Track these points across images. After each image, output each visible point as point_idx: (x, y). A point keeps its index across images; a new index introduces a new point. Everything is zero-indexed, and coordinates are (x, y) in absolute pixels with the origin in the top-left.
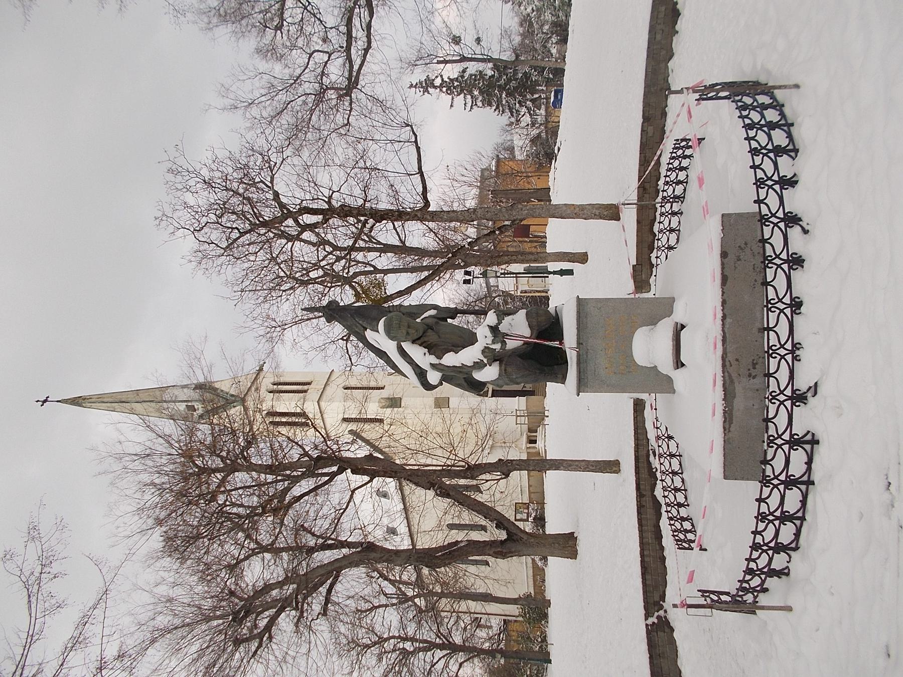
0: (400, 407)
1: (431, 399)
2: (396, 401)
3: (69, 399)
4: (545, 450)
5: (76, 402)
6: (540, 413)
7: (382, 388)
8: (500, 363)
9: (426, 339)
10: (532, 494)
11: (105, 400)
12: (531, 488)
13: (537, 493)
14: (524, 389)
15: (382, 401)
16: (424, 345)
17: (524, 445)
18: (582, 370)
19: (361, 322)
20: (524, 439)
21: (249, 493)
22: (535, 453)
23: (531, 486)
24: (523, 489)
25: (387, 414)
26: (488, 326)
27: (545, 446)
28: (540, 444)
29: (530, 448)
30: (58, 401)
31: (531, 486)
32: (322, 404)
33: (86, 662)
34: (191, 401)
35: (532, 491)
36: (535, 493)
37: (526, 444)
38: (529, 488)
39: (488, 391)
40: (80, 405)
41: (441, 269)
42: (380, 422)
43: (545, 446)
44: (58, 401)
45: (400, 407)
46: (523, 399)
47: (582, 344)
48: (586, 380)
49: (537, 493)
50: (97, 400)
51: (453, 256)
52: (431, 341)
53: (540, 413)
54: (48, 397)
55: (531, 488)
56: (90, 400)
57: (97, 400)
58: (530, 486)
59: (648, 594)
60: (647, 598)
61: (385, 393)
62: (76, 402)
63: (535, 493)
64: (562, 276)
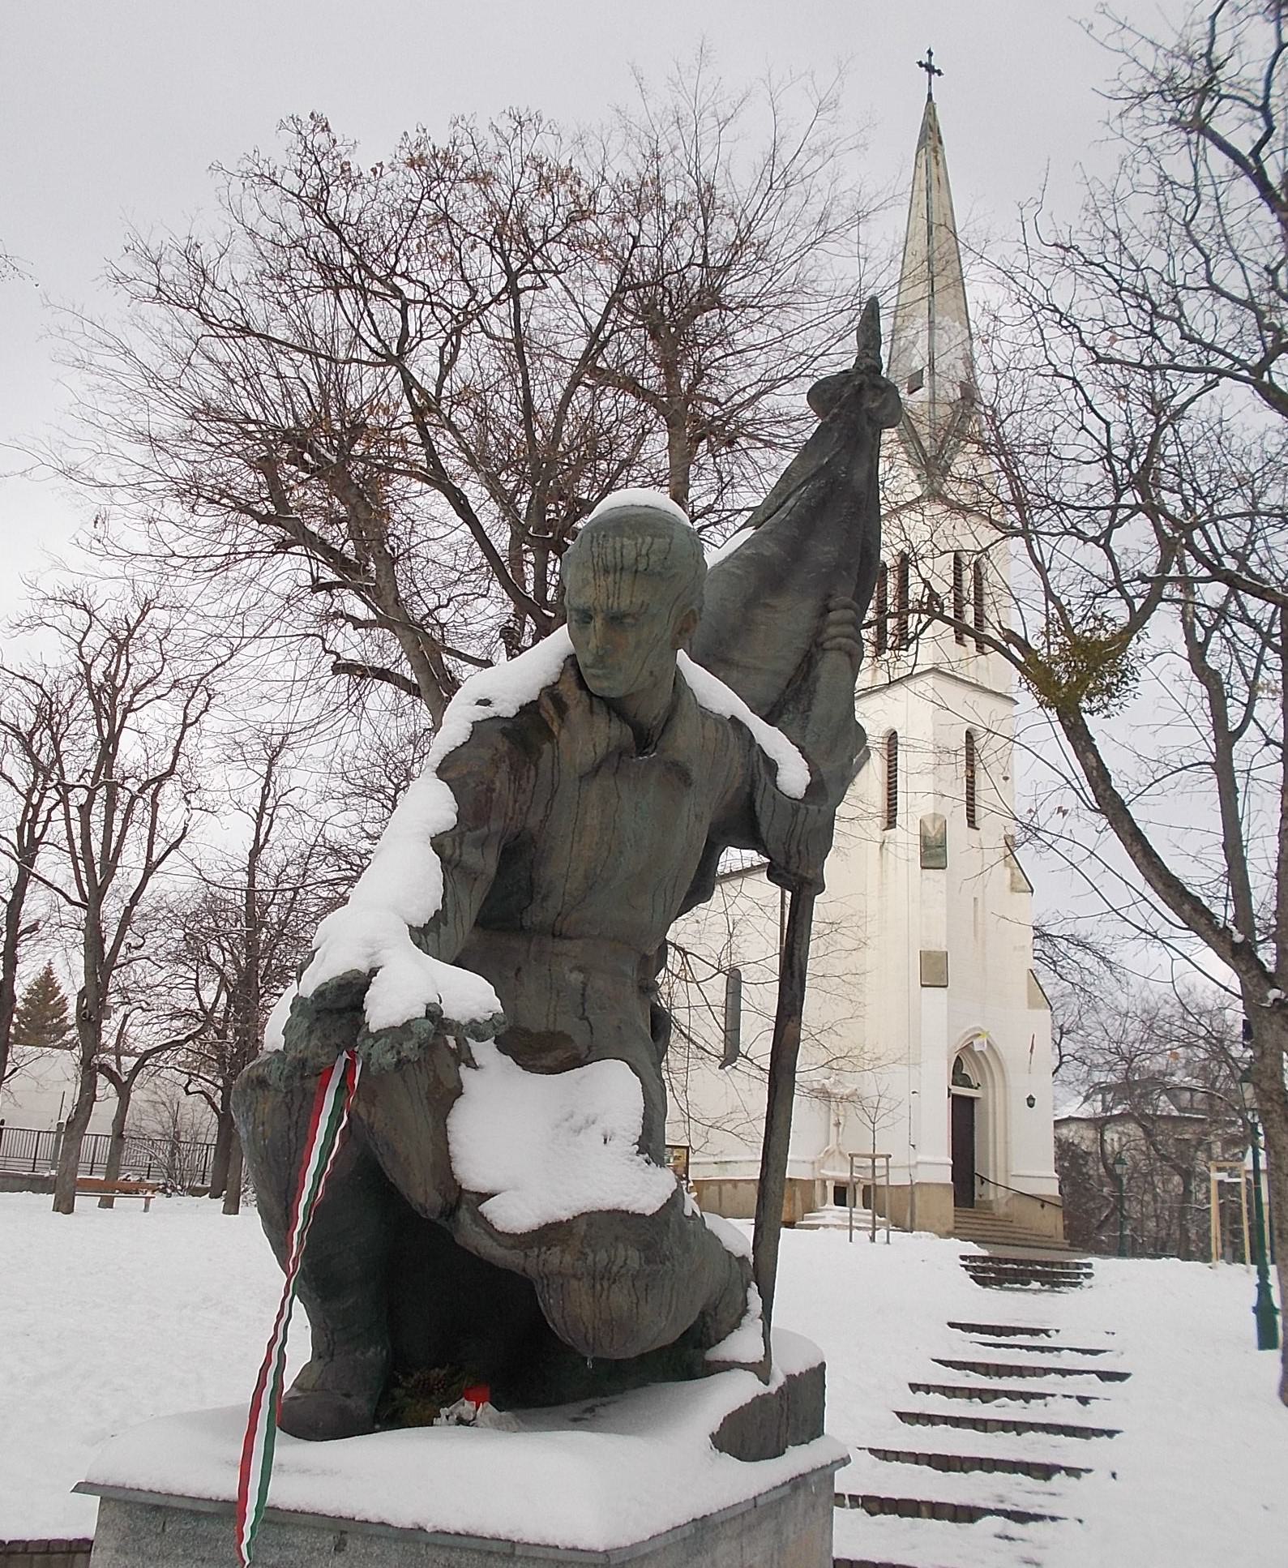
0: (923, 868)
1: (944, 943)
2: (938, 856)
3: (935, 119)
4: (816, 1227)
5: (930, 135)
6: (912, 1220)
7: (972, 823)
8: (468, 1066)
9: (576, 713)
10: (716, 1188)
11: (934, 193)
12: (729, 1186)
13: (720, 1200)
14: (977, 1180)
15: (938, 824)
16: (547, 703)
17: (830, 1173)
18: (205, 1527)
19: (790, 503)
20: (844, 1175)
21: (357, 280)
22: (813, 1201)
23: (735, 1187)
24: (728, 1166)
25: (906, 835)
26: (374, 972)
27: (826, 1226)
28: (832, 1213)
29: (825, 1187)
30: (930, 95)
31: (735, 1187)
32: (930, 679)
33: (726, 480)
34: (932, 381)
35: (723, 1188)
36: (720, 1193)
37: (832, 1178)
38: (730, 1181)
39: (971, 1087)
40: (921, 144)
41: (1186, 907)
42: (889, 822)
43: (826, 1226)
44: (930, 95)
45: (923, 868)
46: (945, 1176)
47: (339, 1547)
48: (154, 1547)
49: (720, 1200)
50: (934, 177)
51: (1234, 945)
52: (564, 736)
53: (912, 1220)
54: (939, 73)
55: (729, 1186)
56: (933, 162)
57: (934, 177)
58: (735, 1183)
59: (37, 1558)
60: (25, 1552)
61: (958, 832)
62: (930, 135)
63: (720, 1193)
64: (1255, 1310)
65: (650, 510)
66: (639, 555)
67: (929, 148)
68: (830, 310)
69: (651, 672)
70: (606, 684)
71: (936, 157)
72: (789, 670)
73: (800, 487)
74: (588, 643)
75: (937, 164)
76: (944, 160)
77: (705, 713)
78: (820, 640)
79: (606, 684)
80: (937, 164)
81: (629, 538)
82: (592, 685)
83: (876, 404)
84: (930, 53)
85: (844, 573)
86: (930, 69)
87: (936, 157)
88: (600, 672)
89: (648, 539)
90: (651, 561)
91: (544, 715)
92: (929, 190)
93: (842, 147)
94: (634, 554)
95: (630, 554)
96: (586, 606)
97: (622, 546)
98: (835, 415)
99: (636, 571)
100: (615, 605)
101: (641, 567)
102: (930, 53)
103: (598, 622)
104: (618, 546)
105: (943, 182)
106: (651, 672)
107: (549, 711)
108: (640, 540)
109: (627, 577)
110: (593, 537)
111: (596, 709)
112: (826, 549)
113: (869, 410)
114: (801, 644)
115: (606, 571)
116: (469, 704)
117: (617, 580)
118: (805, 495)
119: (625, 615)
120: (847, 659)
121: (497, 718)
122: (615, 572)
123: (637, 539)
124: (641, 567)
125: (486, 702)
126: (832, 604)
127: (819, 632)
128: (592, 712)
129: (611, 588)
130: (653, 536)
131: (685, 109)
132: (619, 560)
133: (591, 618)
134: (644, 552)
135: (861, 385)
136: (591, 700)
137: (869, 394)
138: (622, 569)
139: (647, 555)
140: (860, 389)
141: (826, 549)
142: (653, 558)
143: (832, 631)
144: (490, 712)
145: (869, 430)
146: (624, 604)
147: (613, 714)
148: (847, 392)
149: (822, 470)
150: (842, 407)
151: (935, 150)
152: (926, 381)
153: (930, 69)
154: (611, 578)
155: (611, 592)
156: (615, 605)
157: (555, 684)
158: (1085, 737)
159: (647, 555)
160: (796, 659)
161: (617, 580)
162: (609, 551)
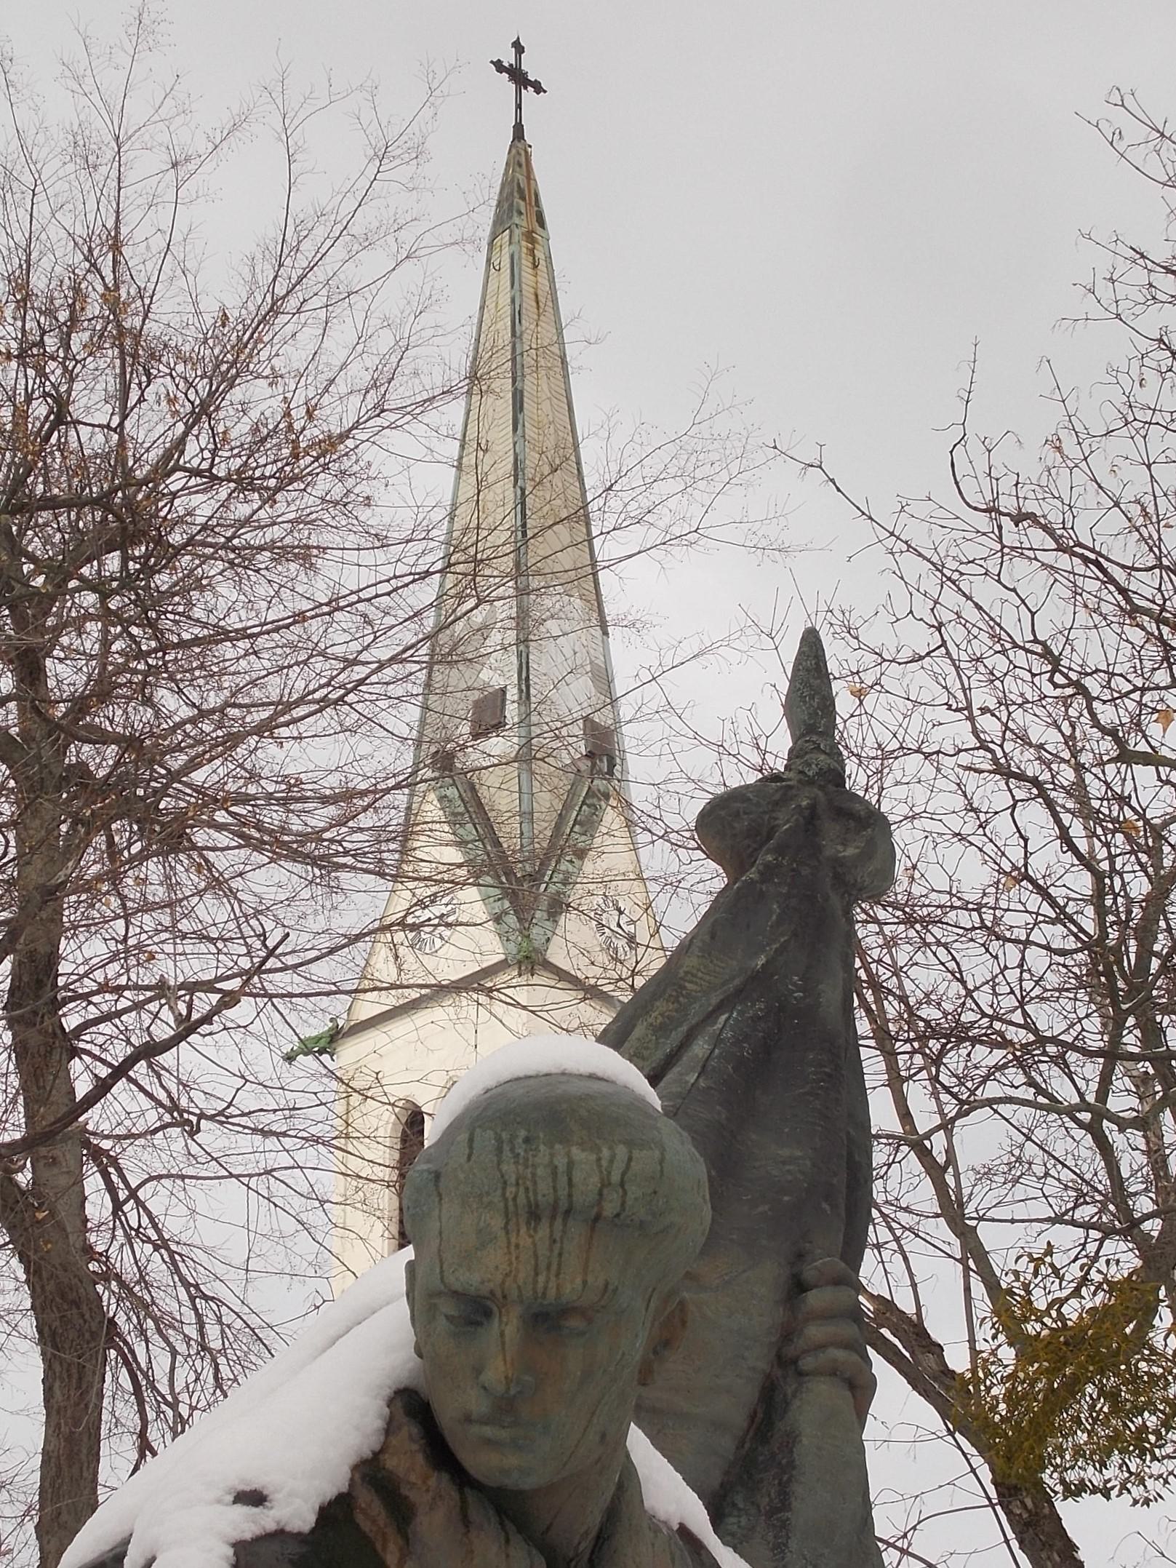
19: (700, 1048)
40: (501, 222)
50: (528, 292)
54: (538, 88)
56: (526, 263)
57: (528, 292)
65: (596, 1086)
66: (605, 1183)
67: (517, 232)
68: (401, 569)
69: (603, 1436)
70: (512, 1460)
71: (532, 252)
72: (739, 1419)
73: (711, 1016)
74: (478, 1371)
75: (535, 267)
76: (549, 258)
77: (655, 1525)
78: (790, 1351)
79: (512, 1460)
80: (535, 267)
81: (581, 1145)
82: (479, 1462)
83: (850, 851)
84: (518, 47)
85: (825, 1206)
86: (518, 77)
87: (532, 252)
88: (503, 1434)
89: (621, 1151)
90: (630, 1196)
91: (366, 1526)
92: (516, 317)
93: (429, 239)
94: (595, 1180)
95: (587, 1181)
96: (484, 1291)
97: (571, 1165)
98: (767, 866)
99: (597, 1218)
100: (552, 1284)
101: (609, 1209)
102: (518, 47)
103: (509, 1326)
104: (561, 1162)
105: (547, 302)
106: (603, 1436)
107: (372, 1513)
108: (606, 1153)
109: (577, 1230)
110: (499, 1141)
111: (475, 1513)
112: (785, 1152)
113: (837, 862)
114: (758, 1360)
115: (534, 1215)
116: (219, 1501)
117: (557, 1235)
118: (728, 1034)
119: (566, 1311)
120: (848, 1394)
121: (279, 1535)
122: (553, 1218)
123: (600, 1150)
124: (609, 1209)
125: (254, 1498)
126: (809, 1274)
127: (787, 1334)
128: (466, 1521)
129: (543, 1251)
130: (630, 1144)
131: (101, 133)
132: (563, 1193)
133: (488, 1314)
134: (615, 1178)
135: (813, 807)
136: (461, 1492)
137: (830, 828)
138: (568, 1212)
139: (622, 1184)
140: (811, 818)
141: (785, 1152)
142: (633, 1191)
143: (815, 1332)
144: (266, 1519)
145: (836, 902)
146: (570, 1287)
147: (511, 1527)
148: (785, 822)
149: (757, 982)
150: (780, 850)
151: (530, 237)
152: (512, 712)
153: (518, 77)
154: (543, 1231)
155: (543, 1265)
156: (552, 1284)
157: (376, 1455)
158: (1059, 1544)
159: (622, 1184)
160: (749, 1393)
161: (557, 1235)
162: (540, 1171)
